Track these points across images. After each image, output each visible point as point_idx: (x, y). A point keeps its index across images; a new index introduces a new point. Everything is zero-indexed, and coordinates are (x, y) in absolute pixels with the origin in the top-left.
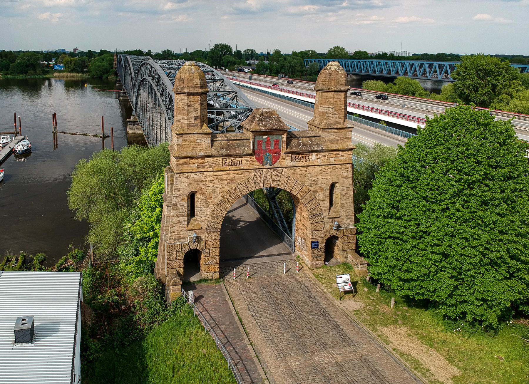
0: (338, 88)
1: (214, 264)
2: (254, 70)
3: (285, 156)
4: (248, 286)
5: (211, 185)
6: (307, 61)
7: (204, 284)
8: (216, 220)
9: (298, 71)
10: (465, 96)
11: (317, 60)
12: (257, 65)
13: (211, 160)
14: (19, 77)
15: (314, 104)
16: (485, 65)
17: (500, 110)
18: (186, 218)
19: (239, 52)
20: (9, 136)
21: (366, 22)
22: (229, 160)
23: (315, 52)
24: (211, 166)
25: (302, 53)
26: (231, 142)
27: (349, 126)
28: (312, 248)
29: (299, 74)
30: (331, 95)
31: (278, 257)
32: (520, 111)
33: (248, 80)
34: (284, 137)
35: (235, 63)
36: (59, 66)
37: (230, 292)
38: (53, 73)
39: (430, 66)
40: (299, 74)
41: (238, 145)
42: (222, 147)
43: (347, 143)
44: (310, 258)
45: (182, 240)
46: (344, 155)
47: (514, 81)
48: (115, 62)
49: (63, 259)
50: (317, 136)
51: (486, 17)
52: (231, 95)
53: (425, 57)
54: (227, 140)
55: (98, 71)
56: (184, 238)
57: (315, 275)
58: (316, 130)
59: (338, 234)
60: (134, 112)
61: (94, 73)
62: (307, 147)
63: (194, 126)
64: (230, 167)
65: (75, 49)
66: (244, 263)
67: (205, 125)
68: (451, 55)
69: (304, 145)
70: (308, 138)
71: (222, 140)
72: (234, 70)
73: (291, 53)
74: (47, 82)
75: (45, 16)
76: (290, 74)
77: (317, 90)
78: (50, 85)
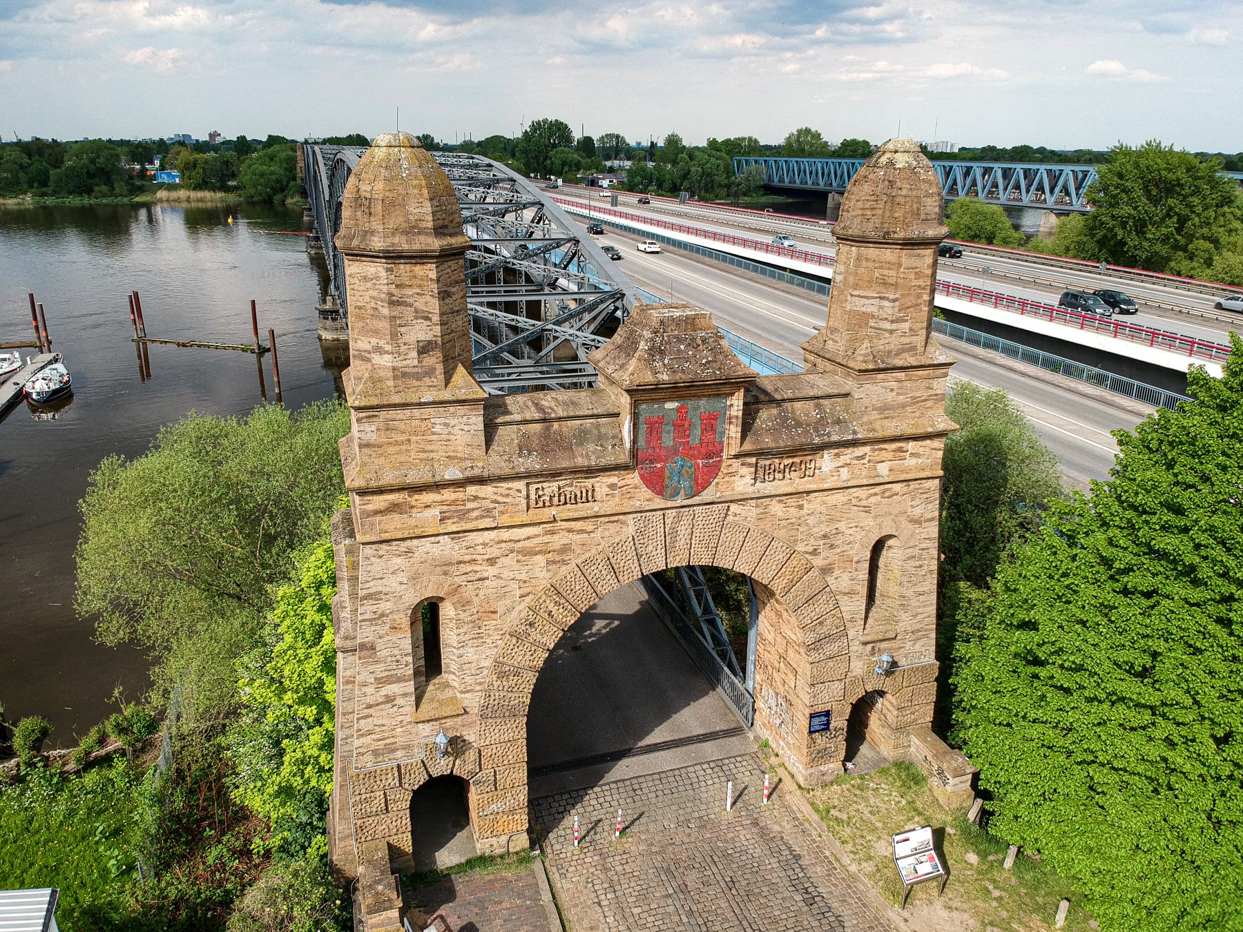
0: (915, 232)
1: (512, 811)
2: (621, 183)
3: (736, 463)
4: (619, 868)
5: (491, 571)
6: (739, 162)
7: (480, 874)
8: (513, 680)
9: (720, 186)
10: (1112, 243)
11: (761, 159)
12: (629, 171)
13: (487, 490)
14: (74, 201)
15: (828, 281)
16: (1166, 169)
17: (1191, 277)
18: (410, 687)
19: (588, 140)
20: (17, 355)
21: (862, 76)
22: (551, 487)
23: (756, 141)
24: (488, 510)
25: (727, 142)
26: (556, 425)
27: (942, 359)
28: (811, 732)
29: (723, 192)
30: (889, 254)
31: (707, 746)
32: (1236, 280)
33: (609, 206)
34: (736, 403)
35: (578, 167)
36: (169, 175)
37: (564, 898)
38: (155, 192)
39: (1006, 174)
40: (723, 192)
41: (582, 437)
42: (524, 448)
43: (930, 413)
44: (805, 759)
45: (399, 754)
46: (921, 451)
47: (1226, 208)
48: (301, 164)
49: (93, 734)
50: (838, 396)
51: (1113, 66)
52: (564, 249)
53: (991, 154)
54: (544, 420)
55: (270, 186)
56: (407, 747)
57: (817, 811)
58: (835, 373)
59: (887, 684)
60: (332, 287)
61: (252, 191)
62: (806, 432)
63: (417, 376)
64: (553, 511)
65: (213, 135)
66: (609, 777)
67: (461, 370)
68: (1042, 150)
69: (798, 424)
70: (812, 403)
71: (525, 422)
72: (577, 182)
73: (703, 143)
74: (143, 214)
75: (139, 55)
76: (703, 193)
77: (842, 239)
78: (151, 219)
